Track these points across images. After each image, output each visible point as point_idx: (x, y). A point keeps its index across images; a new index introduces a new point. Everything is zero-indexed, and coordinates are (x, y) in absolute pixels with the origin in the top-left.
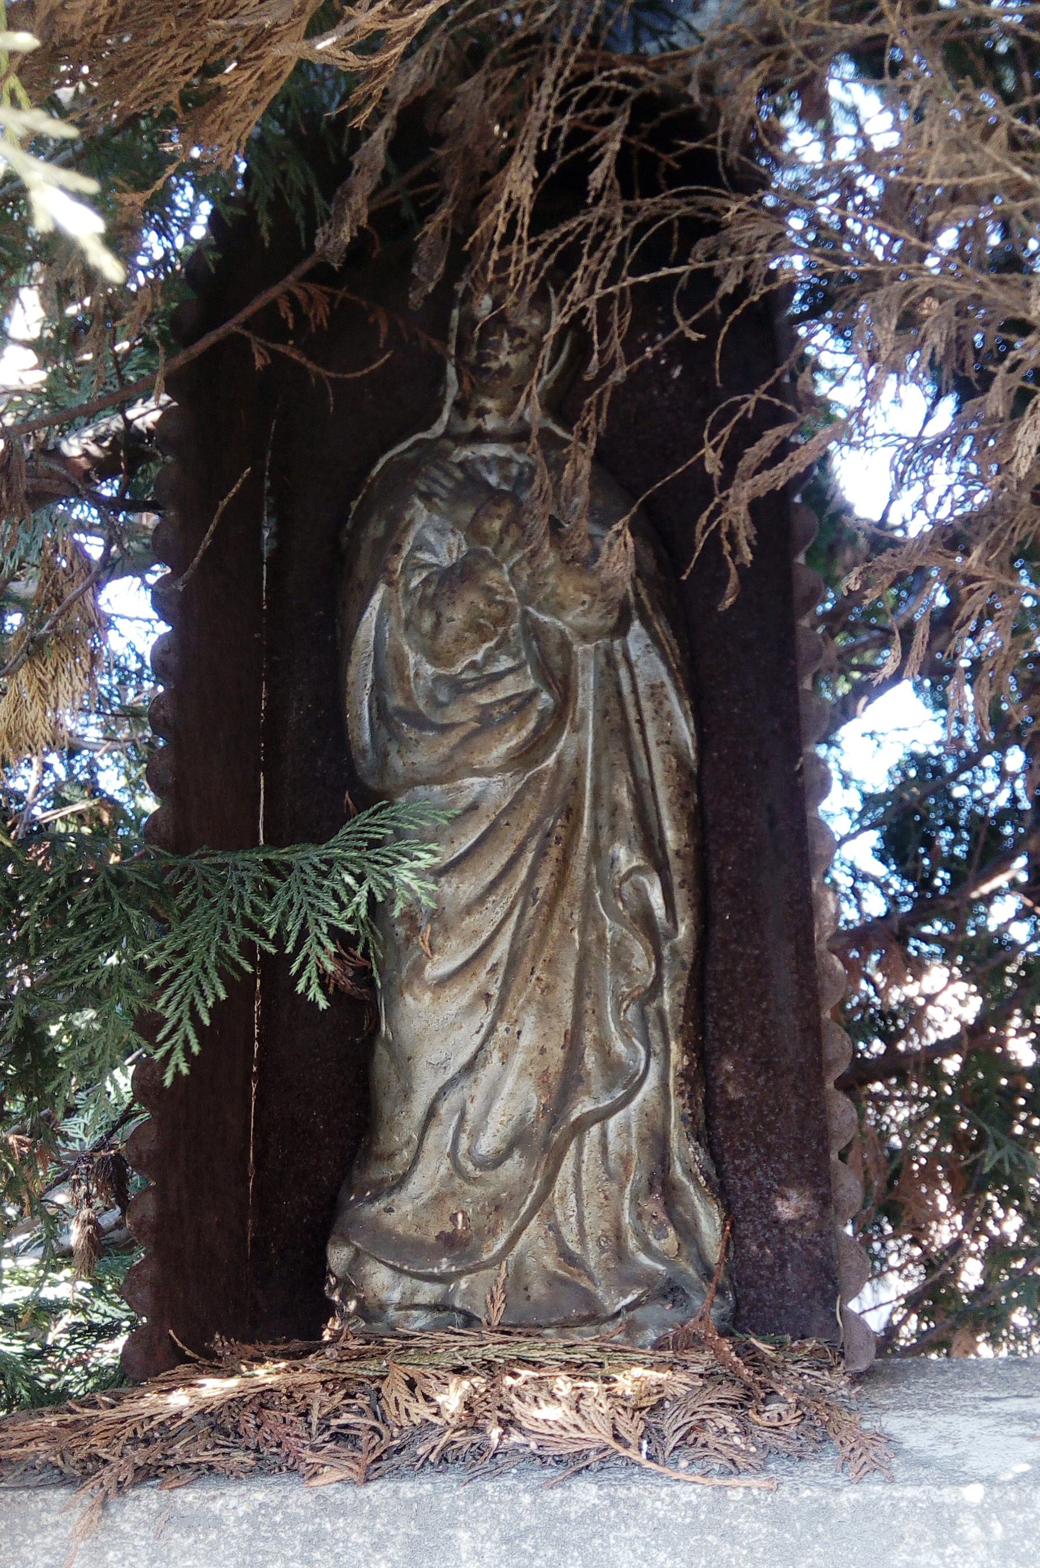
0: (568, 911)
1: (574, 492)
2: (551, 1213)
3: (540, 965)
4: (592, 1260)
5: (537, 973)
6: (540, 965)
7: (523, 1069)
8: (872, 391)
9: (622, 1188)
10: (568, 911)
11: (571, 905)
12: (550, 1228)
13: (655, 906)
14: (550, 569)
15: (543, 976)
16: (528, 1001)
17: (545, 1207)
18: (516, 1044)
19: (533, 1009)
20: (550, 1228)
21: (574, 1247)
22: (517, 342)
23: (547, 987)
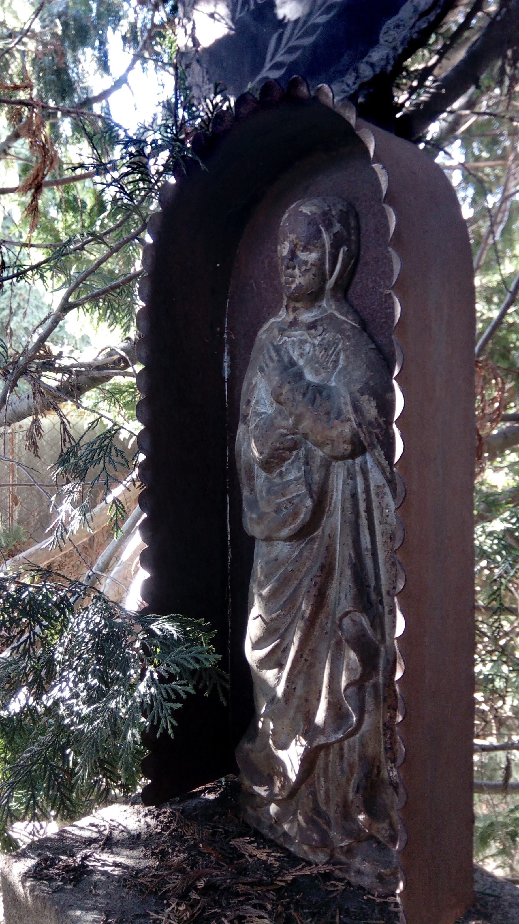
0: (325, 622)
1: (289, 337)
2: (312, 784)
3: (307, 652)
4: (332, 814)
5: (305, 657)
6: (307, 652)
7: (298, 707)
8: (312, 296)
9: (348, 781)
10: (324, 623)
11: (327, 618)
12: (311, 793)
13: (370, 576)
14: (157, 149)
15: (309, 658)
16: (300, 672)
17: (309, 780)
18: (293, 694)
19: (302, 676)
20: (311, 793)
21: (324, 807)
22: (303, 268)
23: (310, 665)
